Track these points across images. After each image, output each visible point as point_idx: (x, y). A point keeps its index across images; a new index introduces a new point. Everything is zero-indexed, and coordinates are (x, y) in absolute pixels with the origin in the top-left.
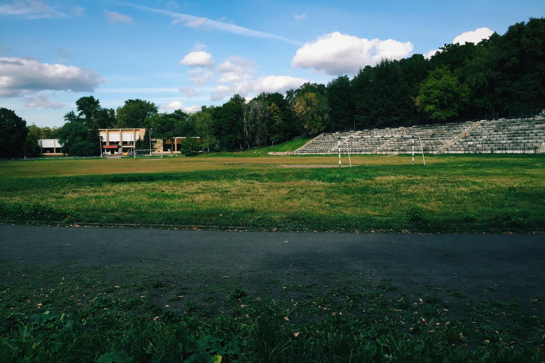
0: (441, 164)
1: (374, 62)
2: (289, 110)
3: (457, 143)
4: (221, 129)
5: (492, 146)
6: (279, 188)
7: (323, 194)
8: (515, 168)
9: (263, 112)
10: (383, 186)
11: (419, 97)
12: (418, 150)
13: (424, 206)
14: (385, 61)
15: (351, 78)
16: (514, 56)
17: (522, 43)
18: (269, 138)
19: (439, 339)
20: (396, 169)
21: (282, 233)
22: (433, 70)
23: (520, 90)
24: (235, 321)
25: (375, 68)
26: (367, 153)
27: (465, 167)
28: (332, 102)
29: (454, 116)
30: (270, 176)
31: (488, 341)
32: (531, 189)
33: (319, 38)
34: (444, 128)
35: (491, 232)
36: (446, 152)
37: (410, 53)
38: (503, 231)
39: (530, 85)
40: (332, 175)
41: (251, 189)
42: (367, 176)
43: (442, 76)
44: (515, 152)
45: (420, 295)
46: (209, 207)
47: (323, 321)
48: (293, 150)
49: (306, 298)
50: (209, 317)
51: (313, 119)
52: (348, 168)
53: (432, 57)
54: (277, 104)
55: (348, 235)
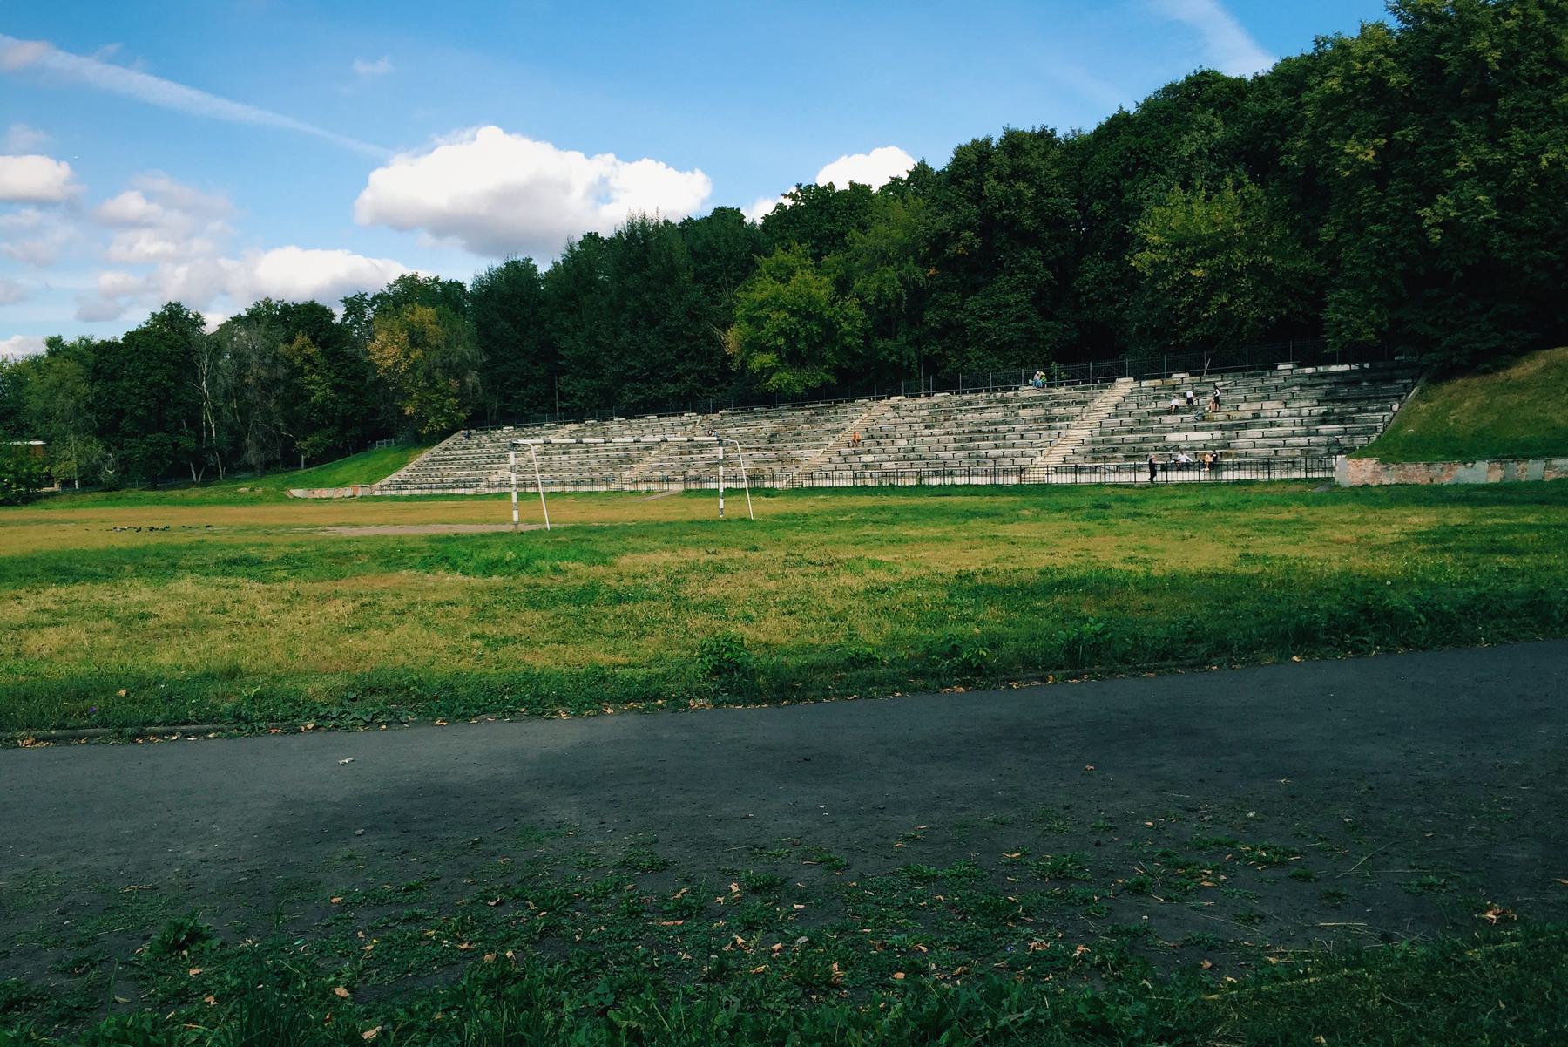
0: (794, 516)
1: (609, 221)
2: (355, 359)
3: (836, 459)
4: (120, 414)
5: (920, 465)
6: (324, 599)
7: (464, 611)
8: (972, 523)
9: (268, 361)
10: (639, 581)
11: (735, 328)
12: (735, 479)
13: (749, 632)
14: (638, 220)
15: (543, 268)
16: (969, 227)
17: (986, 193)
18: (288, 446)
19: (778, 988)
20: (674, 533)
21: (332, 735)
22: (767, 256)
23: (985, 319)
24: (167, 1023)
25: (611, 240)
26: (597, 488)
27: (856, 523)
28: (487, 337)
29: (825, 384)
30: (295, 564)
31: (901, 975)
32: (1009, 574)
33: (437, 140)
34: (800, 417)
35: (915, 690)
36: (806, 484)
37: (704, 202)
38: (942, 686)
39: (1008, 305)
40: (493, 554)
41: (228, 607)
42: (595, 553)
43: (792, 273)
44: (974, 480)
45: (732, 874)
46: (80, 670)
47: (457, 982)
48: (371, 481)
49: (407, 921)
50: (74, 1021)
51: (432, 385)
52: (540, 532)
53: (767, 218)
54: (314, 339)
55: (537, 726)
